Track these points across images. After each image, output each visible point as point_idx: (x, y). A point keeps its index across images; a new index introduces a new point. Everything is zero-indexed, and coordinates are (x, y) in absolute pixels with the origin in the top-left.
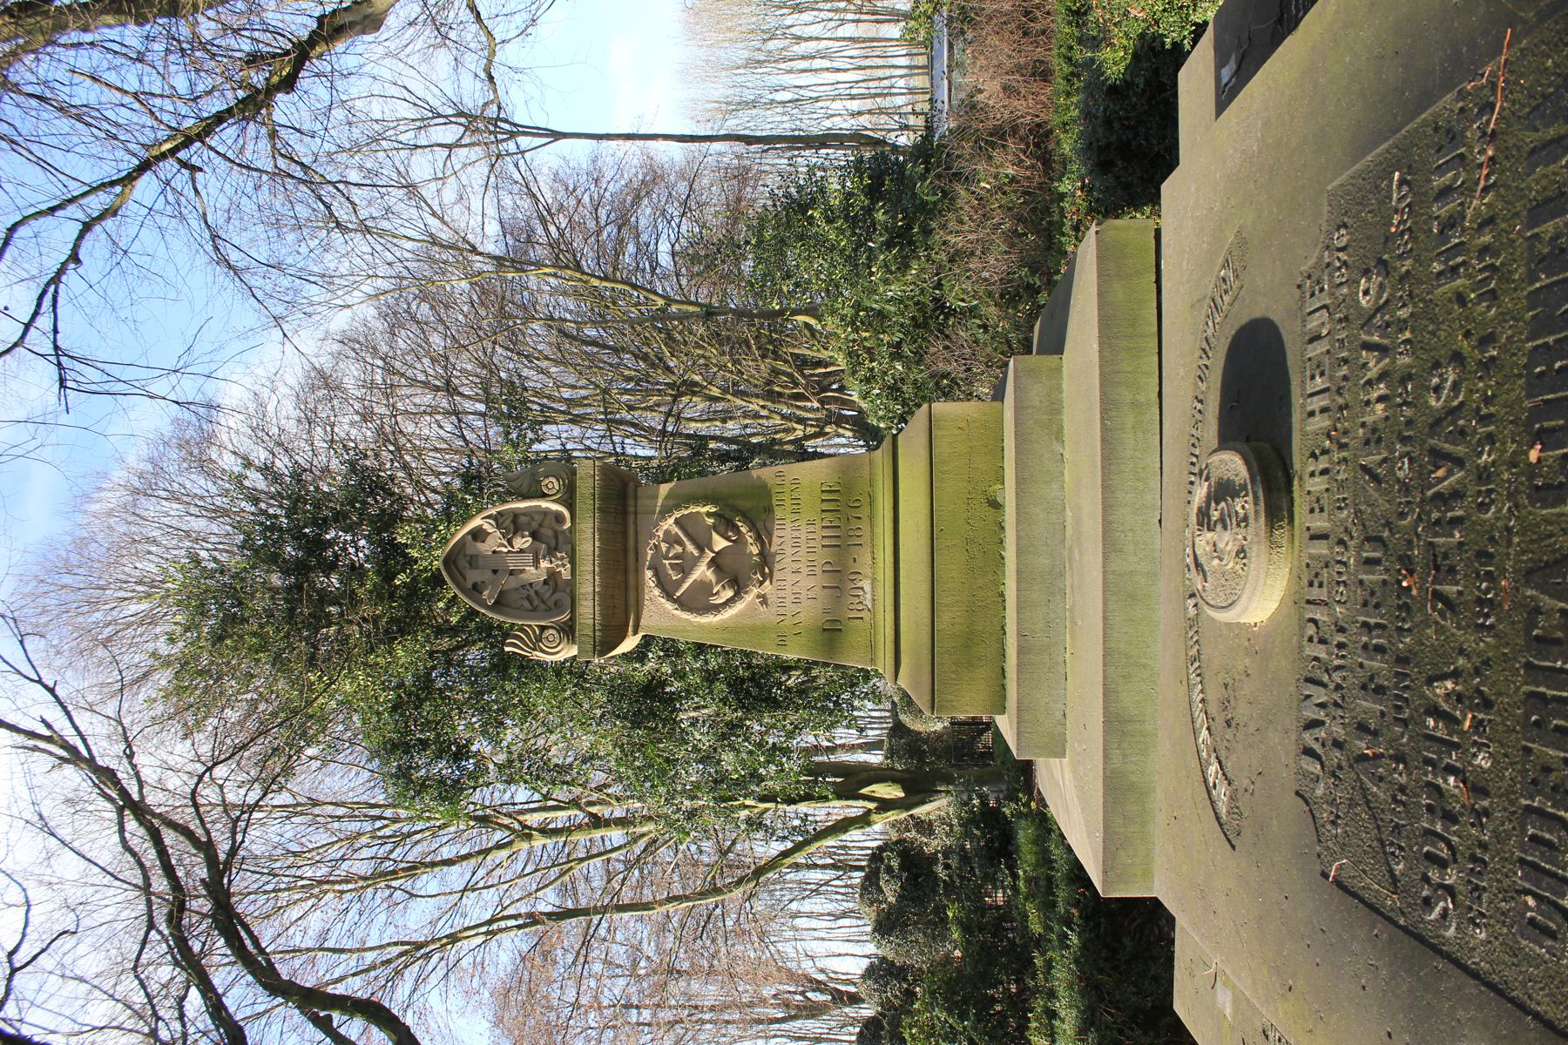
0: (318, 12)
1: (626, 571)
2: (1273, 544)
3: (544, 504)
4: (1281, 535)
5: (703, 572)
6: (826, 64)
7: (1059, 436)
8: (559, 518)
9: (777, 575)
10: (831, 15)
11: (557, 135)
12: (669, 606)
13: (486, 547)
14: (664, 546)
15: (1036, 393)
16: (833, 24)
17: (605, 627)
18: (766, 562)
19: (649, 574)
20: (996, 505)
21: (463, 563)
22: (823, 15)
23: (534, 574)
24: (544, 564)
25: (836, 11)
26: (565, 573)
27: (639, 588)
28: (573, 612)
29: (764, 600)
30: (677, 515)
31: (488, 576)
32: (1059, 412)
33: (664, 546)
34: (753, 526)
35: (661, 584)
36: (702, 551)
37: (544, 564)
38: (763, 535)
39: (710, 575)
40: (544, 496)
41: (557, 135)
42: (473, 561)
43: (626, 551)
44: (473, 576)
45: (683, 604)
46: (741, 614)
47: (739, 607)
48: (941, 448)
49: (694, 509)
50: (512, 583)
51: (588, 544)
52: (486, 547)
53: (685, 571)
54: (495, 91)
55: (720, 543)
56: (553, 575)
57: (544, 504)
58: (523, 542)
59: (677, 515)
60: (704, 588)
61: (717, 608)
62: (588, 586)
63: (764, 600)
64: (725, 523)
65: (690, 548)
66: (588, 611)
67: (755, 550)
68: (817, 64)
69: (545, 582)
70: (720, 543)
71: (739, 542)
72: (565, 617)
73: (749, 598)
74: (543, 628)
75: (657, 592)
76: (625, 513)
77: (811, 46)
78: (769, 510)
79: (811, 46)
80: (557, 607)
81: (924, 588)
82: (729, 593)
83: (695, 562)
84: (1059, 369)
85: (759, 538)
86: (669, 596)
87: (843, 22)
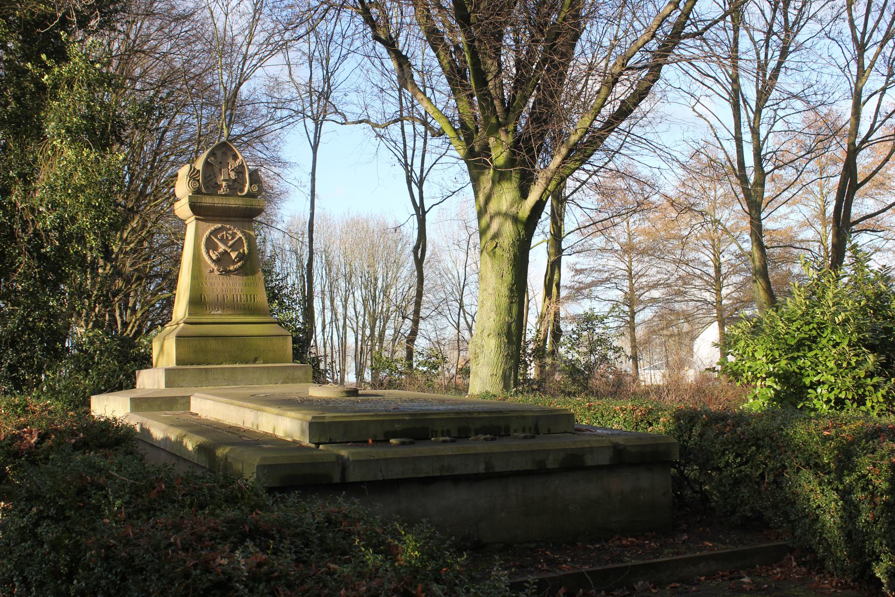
0: (409, 56)
1: (221, 216)
2: (342, 392)
3: (247, 185)
4: (344, 394)
5: (222, 247)
6: (328, 321)
7: (285, 382)
8: (242, 190)
9: (221, 277)
10: (360, 324)
11: (315, 148)
12: (207, 233)
13: (231, 161)
14: (230, 232)
15: (299, 374)
16: (355, 325)
17: (201, 207)
18: (227, 273)
19: (220, 225)
20: (255, 361)
21: (224, 149)
22: (361, 319)
23: (221, 179)
24: (224, 184)
25: (364, 326)
26: (221, 191)
27: (214, 221)
28: (205, 194)
29: (212, 271)
30: (243, 238)
31: (219, 160)
32: (293, 382)
33: (230, 232)
34: (240, 268)
35: (216, 230)
36: (230, 247)
37: (224, 184)
38: (237, 272)
39: (221, 250)
40: (251, 185)
41: (315, 148)
42: (225, 154)
43: (228, 216)
44: (219, 153)
45: (209, 239)
46: (206, 263)
47: (209, 262)
48: (275, 339)
49: (246, 245)
50: (217, 170)
51: (233, 202)
52: (231, 161)
53: (222, 240)
54: (353, 123)
55: (233, 255)
56: (220, 186)
57: (247, 185)
58: (233, 175)
59: (243, 238)
60: (215, 248)
61: (208, 253)
62: (217, 202)
63: (212, 271)
64: (241, 257)
65: (231, 243)
66: (207, 201)
67: (232, 268)
68: (328, 314)
69: (216, 183)
70: (233, 255)
71: (234, 263)
72: (203, 190)
73: (213, 265)
74: (198, 181)
75: (213, 228)
76: (243, 217)
77: (340, 310)
78: (246, 274)
79: (340, 310)
80: (207, 188)
81: (231, 333)
82: (214, 258)
83: (226, 244)
84: (307, 382)
85: (236, 270)
86: (211, 233)
87: (356, 333)
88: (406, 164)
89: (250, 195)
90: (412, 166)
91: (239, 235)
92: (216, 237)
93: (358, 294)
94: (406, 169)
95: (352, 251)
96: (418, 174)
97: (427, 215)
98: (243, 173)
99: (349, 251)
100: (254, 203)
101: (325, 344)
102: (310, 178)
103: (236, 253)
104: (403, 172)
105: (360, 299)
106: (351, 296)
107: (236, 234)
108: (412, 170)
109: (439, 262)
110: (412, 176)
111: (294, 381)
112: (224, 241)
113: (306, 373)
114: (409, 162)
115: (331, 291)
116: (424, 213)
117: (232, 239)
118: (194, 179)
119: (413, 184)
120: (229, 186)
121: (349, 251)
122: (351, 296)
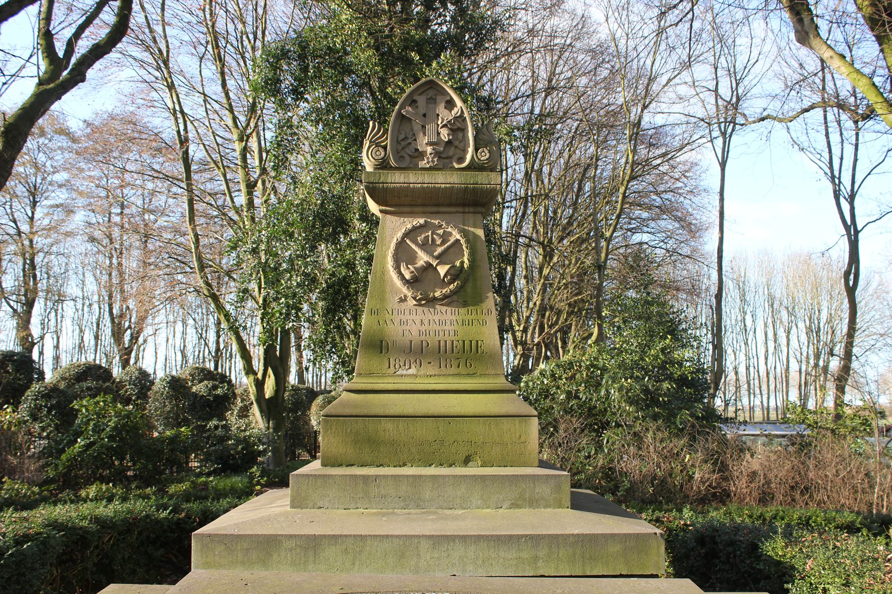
3: (471, 150)
5: (423, 258)
7: (514, 505)
8: (461, 160)
9: (420, 309)
10: (805, 354)
11: (723, 165)
12: (399, 235)
13: (441, 110)
14: (441, 232)
15: (544, 490)
18: (428, 301)
20: (467, 461)
21: (431, 93)
22: (805, 349)
23: (423, 143)
24: (429, 149)
26: (423, 164)
27: (412, 214)
28: (396, 169)
29: (403, 300)
30: (462, 241)
31: (422, 111)
33: (441, 232)
34: (454, 293)
36: (437, 258)
37: (429, 149)
38: (447, 300)
39: (420, 263)
40: (476, 149)
41: (723, 165)
42: (432, 101)
43: (438, 205)
44: (421, 100)
45: (401, 244)
46: (393, 284)
47: (398, 283)
48: (506, 424)
50: (417, 127)
51: (443, 179)
52: (441, 110)
53: (424, 246)
55: (442, 270)
56: (421, 155)
57: (471, 150)
58: (445, 134)
59: (462, 241)
60: (412, 259)
62: (413, 179)
64: (456, 274)
65: (439, 250)
66: (397, 179)
67: (437, 294)
68: (771, 344)
69: (417, 150)
70: (442, 270)
71: (443, 284)
72: (393, 163)
73: (405, 290)
74: (385, 148)
75: (409, 226)
76: (464, 205)
78: (465, 304)
79: (783, 339)
80: (399, 158)
81: (410, 411)
82: (408, 276)
83: (430, 253)
84: (560, 506)
85: (445, 297)
86: (407, 235)
88: (833, 177)
89: (474, 167)
90: (839, 178)
91: (456, 235)
92: (415, 242)
93: (801, 325)
94: (833, 182)
95: (795, 284)
96: (849, 189)
97: (860, 235)
98: (464, 130)
99: (791, 285)
100: (483, 179)
101: (768, 374)
102: (718, 197)
103: (447, 267)
104: (830, 187)
105: (804, 330)
106: (794, 328)
107: (450, 234)
108: (840, 182)
109: (887, 293)
110: (840, 190)
111: (533, 503)
112: (426, 246)
113: (558, 488)
114: (836, 173)
115: (774, 323)
116: (857, 232)
117: (443, 243)
118: (378, 145)
119: (842, 200)
120: (437, 154)
121: (791, 285)
122: (794, 328)
